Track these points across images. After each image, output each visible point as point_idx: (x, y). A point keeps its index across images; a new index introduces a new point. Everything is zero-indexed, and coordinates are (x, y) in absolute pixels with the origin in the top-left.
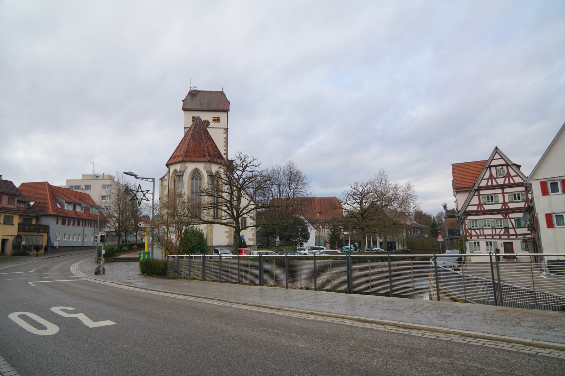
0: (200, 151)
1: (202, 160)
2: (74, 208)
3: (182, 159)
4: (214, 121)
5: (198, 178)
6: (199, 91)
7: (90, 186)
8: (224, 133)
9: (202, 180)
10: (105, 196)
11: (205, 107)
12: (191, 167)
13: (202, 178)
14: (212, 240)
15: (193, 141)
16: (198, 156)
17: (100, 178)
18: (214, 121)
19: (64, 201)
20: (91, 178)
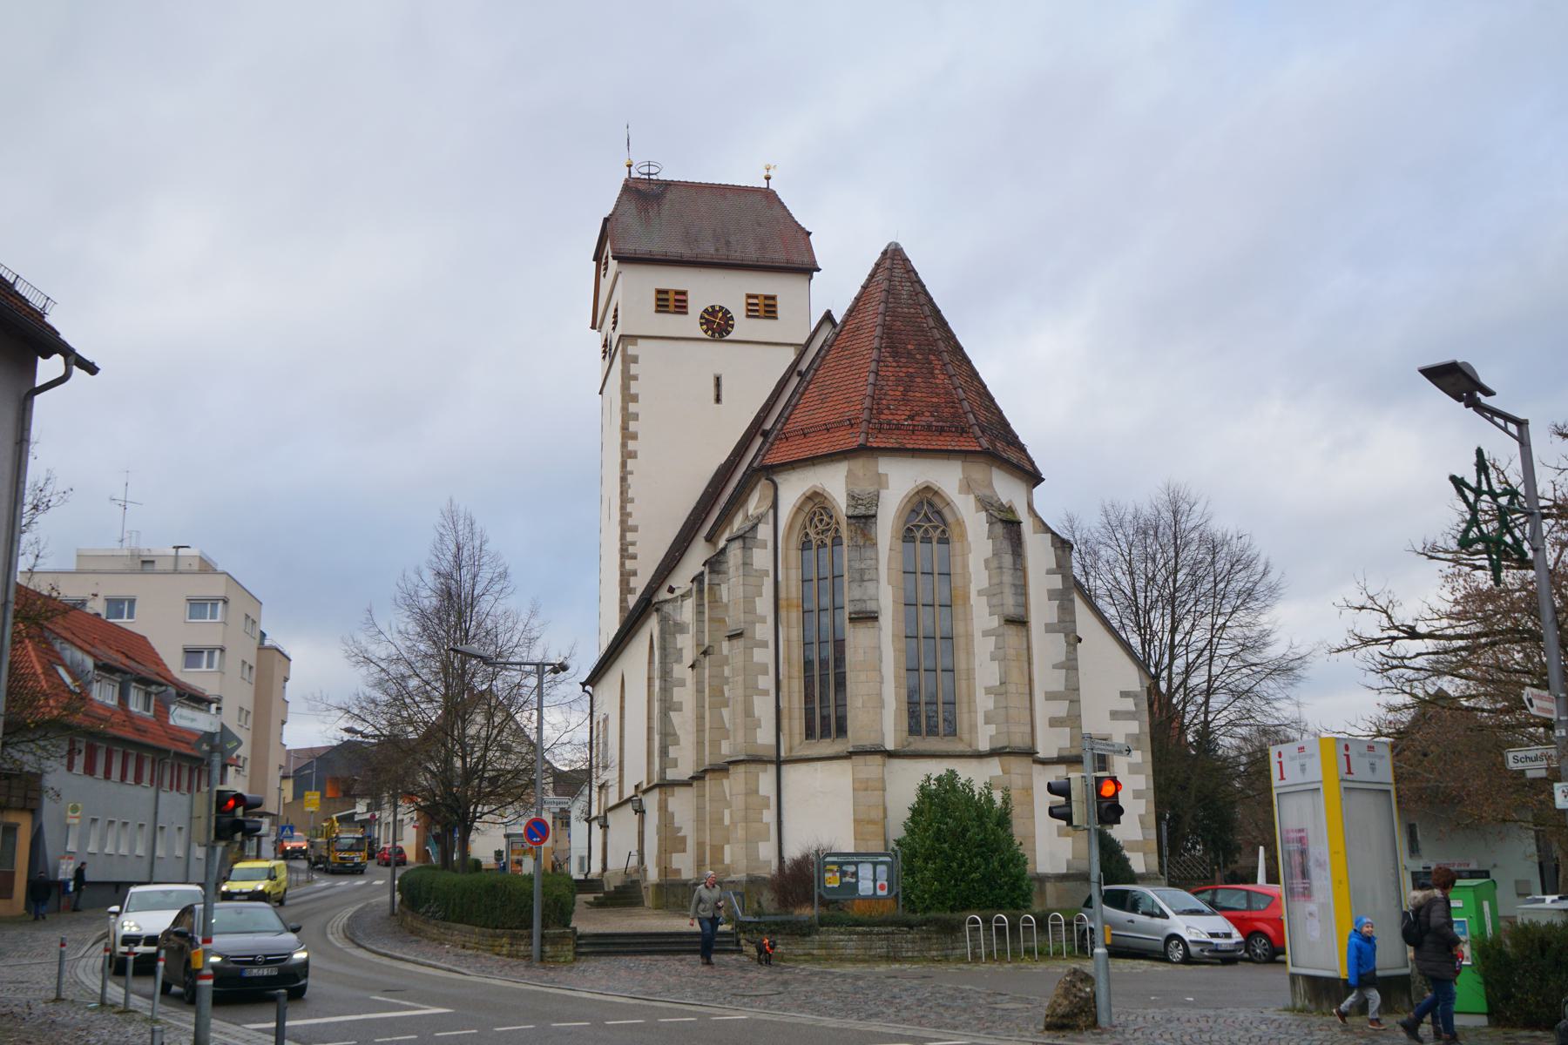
0: (938, 406)
1: (952, 444)
2: (123, 697)
3: (861, 440)
4: (752, 312)
5: (936, 535)
6: (668, 185)
7: (132, 602)
9: (956, 546)
10: (199, 652)
11: (708, 250)
12: (899, 480)
13: (953, 533)
14: (1035, 863)
15: (895, 354)
16: (929, 427)
17: (158, 567)
18: (752, 312)
19: (89, 663)
20: (120, 567)
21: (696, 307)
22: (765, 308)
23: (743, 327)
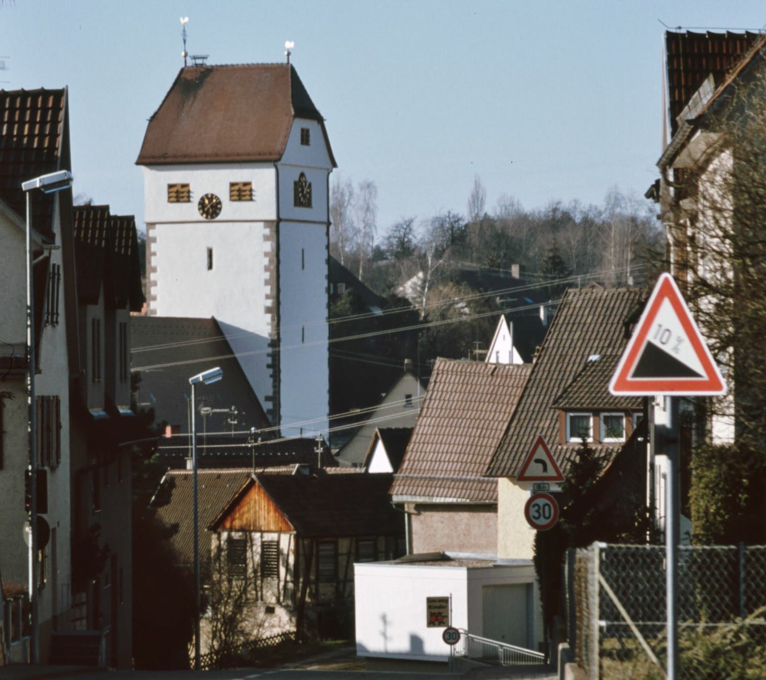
8: (266, 238)
21: (196, 198)
22: (242, 192)
23: (229, 209)
